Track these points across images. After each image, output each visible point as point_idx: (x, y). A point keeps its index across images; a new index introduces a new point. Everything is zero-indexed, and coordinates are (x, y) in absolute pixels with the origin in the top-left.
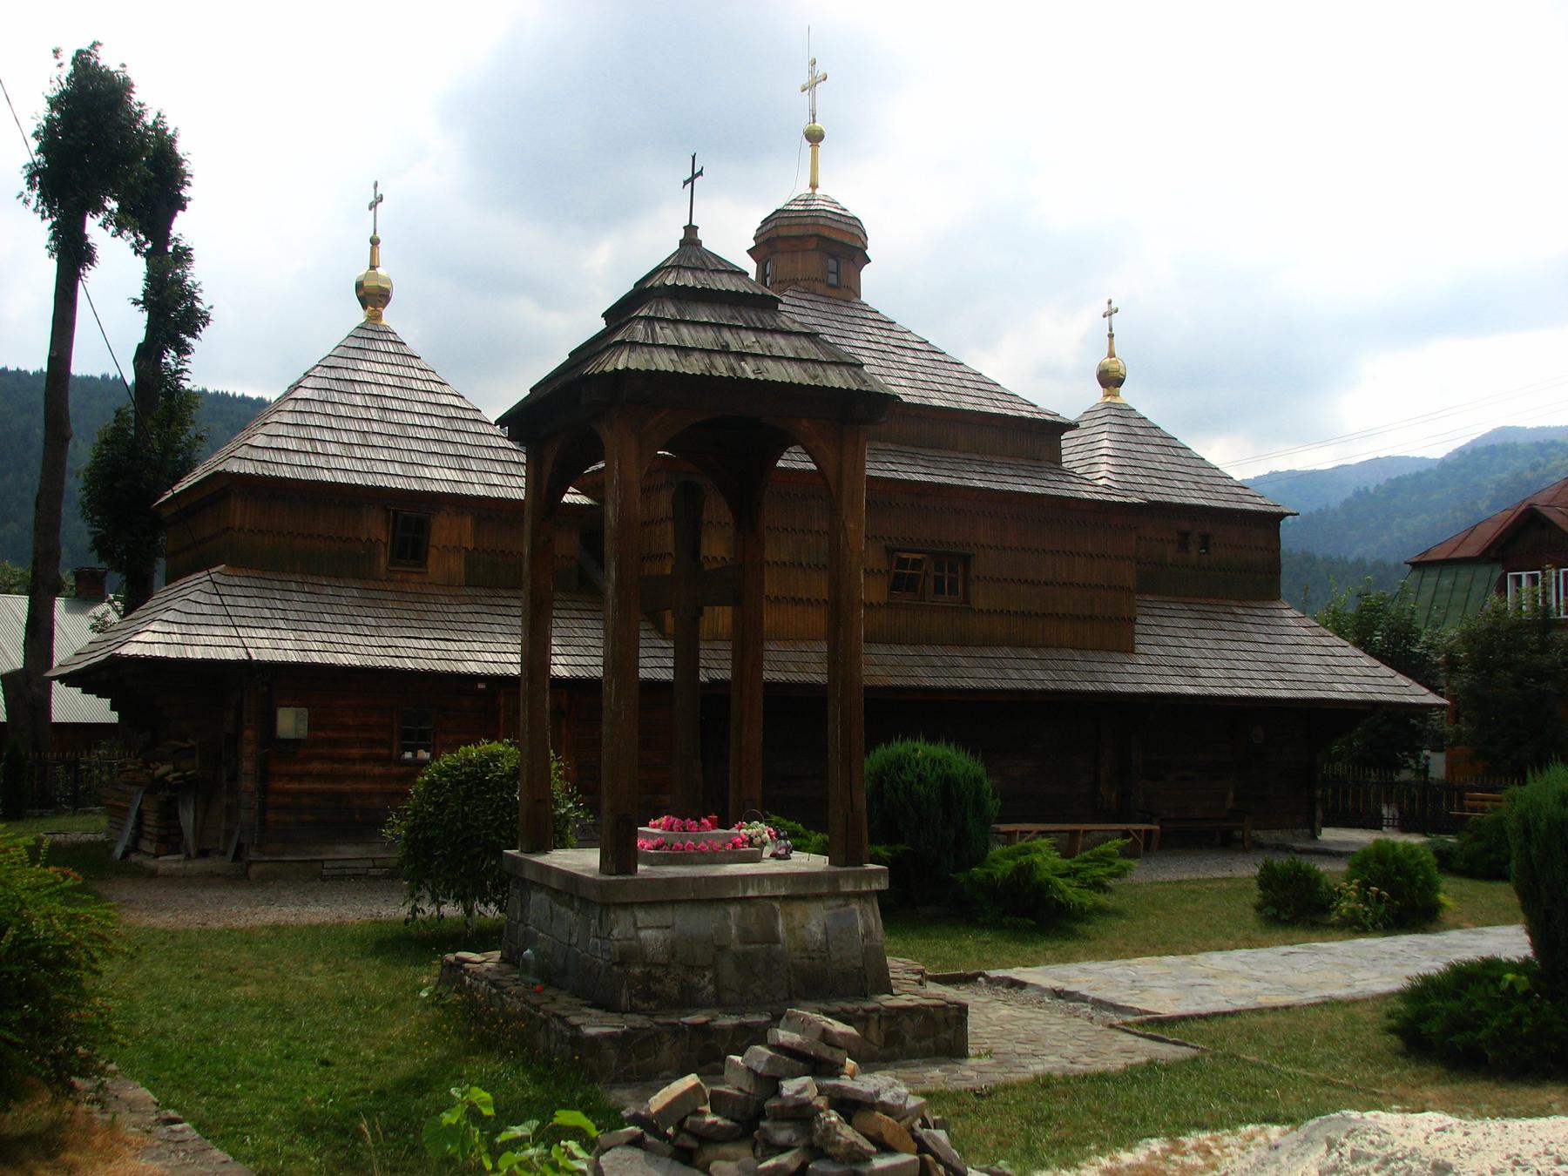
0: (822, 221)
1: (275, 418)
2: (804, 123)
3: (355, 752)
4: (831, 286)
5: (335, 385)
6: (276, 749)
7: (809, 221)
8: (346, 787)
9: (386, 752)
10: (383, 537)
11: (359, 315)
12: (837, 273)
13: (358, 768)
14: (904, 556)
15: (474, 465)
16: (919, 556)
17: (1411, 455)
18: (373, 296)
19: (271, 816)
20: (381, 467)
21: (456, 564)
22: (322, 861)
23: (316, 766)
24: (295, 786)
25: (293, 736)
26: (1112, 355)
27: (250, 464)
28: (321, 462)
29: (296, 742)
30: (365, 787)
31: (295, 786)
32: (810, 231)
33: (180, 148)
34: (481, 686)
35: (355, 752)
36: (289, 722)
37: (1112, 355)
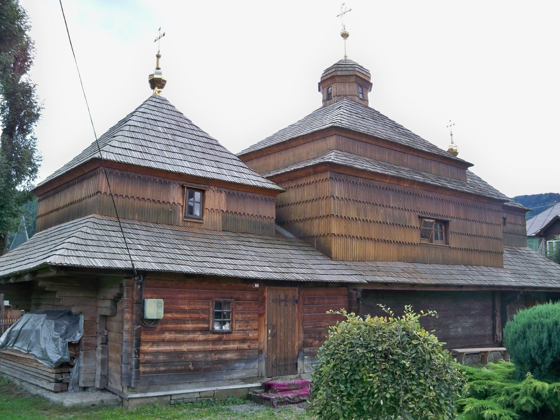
0: (357, 69)
1: (120, 133)
2: (340, 31)
3: (190, 326)
4: (360, 99)
5: (147, 121)
6: (146, 325)
7: (351, 69)
8: (184, 348)
9: (206, 326)
10: (181, 202)
11: (149, 92)
12: (362, 94)
13: (191, 336)
14: (427, 220)
15: (225, 166)
16: (432, 221)
17: (536, 194)
18: (156, 83)
19: (142, 369)
20: (180, 163)
21: (218, 218)
22: (171, 395)
23: (167, 336)
24: (155, 348)
25: (155, 317)
26: (452, 143)
27: (153, 132)
28: (149, 157)
29: (156, 321)
30: (195, 347)
31: (155, 348)
32: (351, 73)
33: (31, 53)
34: (257, 285)
35: (190, 326)
36: (154, 308)
37: (452, 143)
